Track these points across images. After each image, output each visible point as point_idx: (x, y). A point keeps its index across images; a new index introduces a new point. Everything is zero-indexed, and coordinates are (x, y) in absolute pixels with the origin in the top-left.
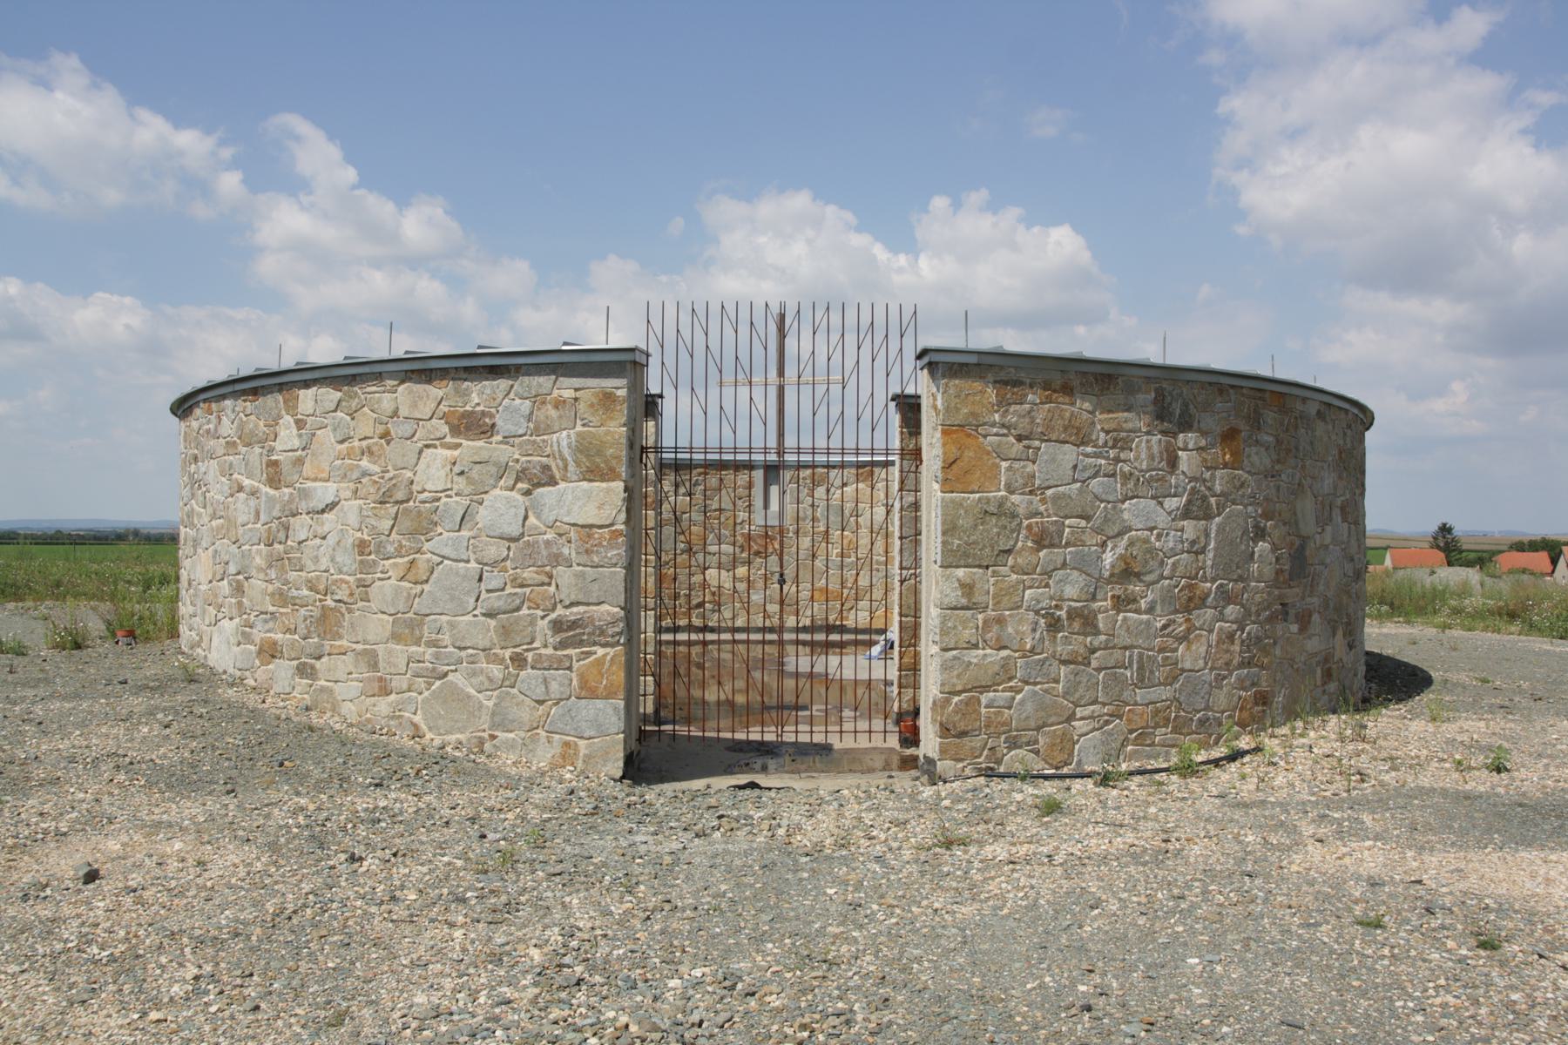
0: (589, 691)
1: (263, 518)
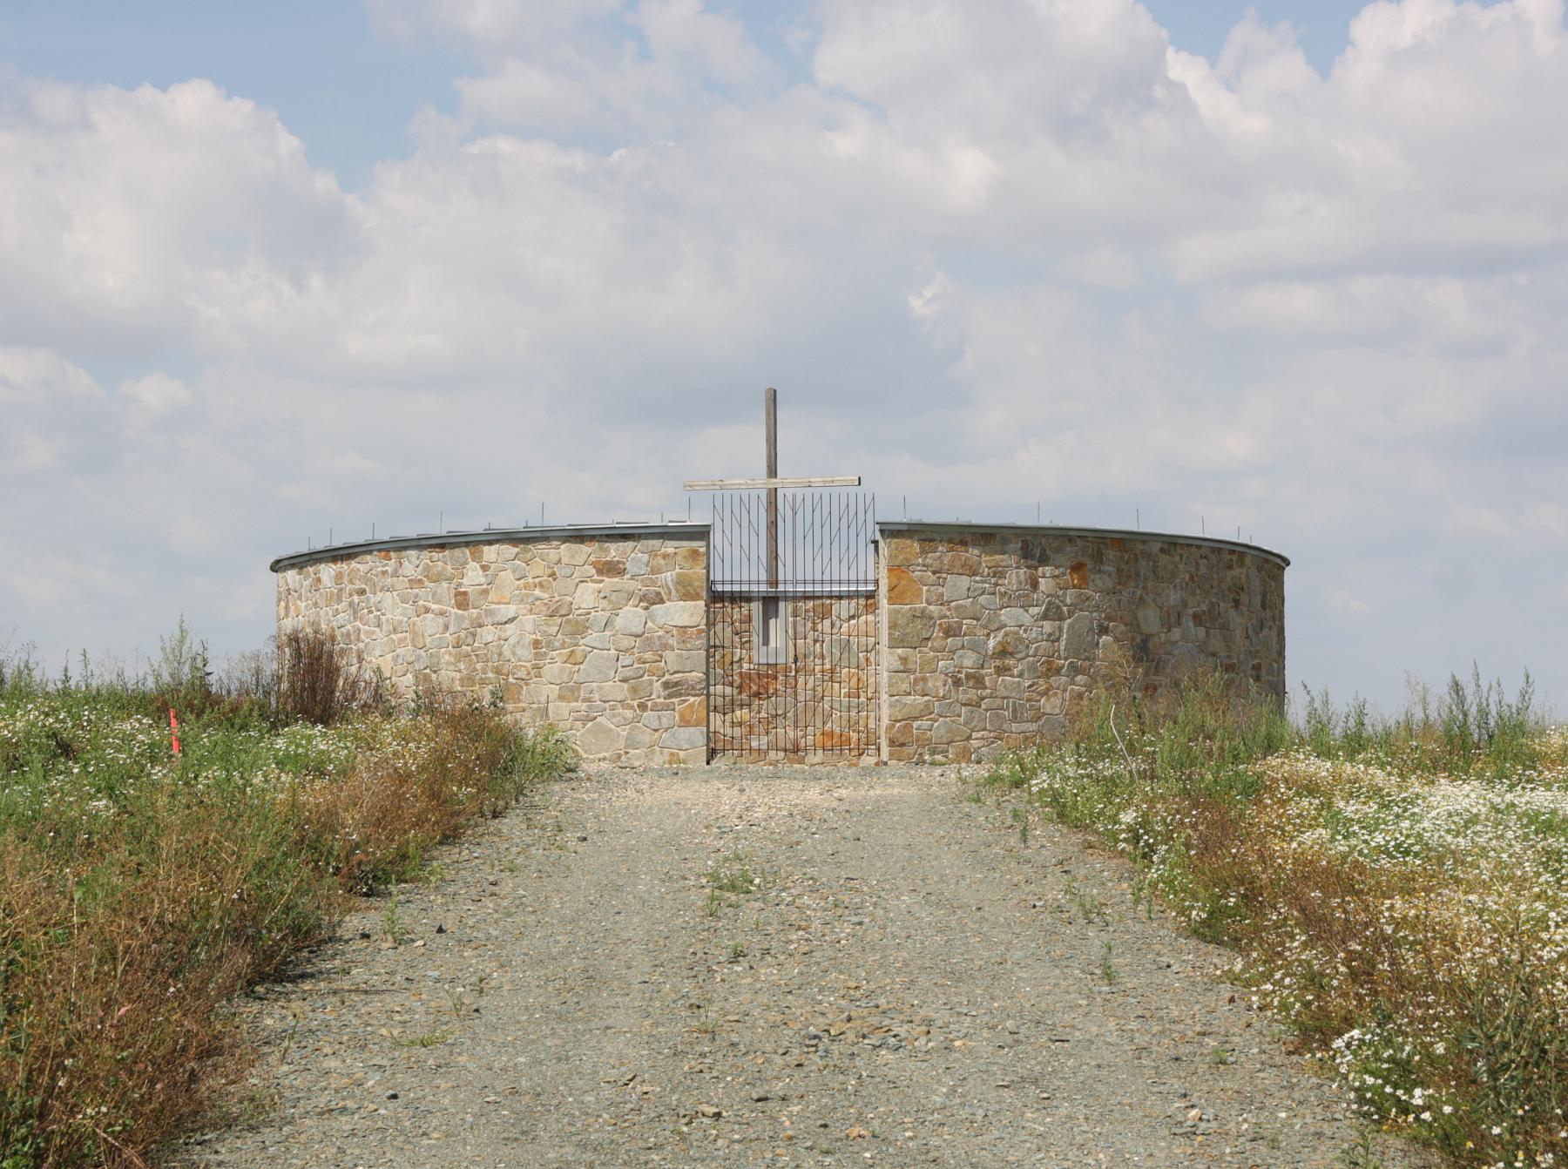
0: (685, 723)
1: (452, 629)
